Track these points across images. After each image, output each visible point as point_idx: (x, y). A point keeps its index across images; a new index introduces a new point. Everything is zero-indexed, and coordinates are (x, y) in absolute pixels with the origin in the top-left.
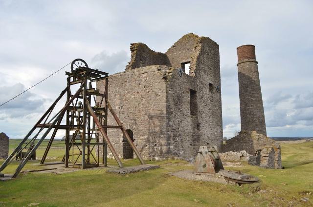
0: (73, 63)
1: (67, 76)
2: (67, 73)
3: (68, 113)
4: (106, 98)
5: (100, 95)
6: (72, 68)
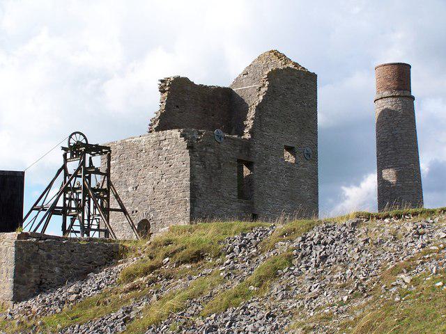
0: (70, 137)
1: (63, 152)
2: (63, 148)
3: (65, 195)
4: (109, 177)
5: (101, 174)
6: (69, 143)
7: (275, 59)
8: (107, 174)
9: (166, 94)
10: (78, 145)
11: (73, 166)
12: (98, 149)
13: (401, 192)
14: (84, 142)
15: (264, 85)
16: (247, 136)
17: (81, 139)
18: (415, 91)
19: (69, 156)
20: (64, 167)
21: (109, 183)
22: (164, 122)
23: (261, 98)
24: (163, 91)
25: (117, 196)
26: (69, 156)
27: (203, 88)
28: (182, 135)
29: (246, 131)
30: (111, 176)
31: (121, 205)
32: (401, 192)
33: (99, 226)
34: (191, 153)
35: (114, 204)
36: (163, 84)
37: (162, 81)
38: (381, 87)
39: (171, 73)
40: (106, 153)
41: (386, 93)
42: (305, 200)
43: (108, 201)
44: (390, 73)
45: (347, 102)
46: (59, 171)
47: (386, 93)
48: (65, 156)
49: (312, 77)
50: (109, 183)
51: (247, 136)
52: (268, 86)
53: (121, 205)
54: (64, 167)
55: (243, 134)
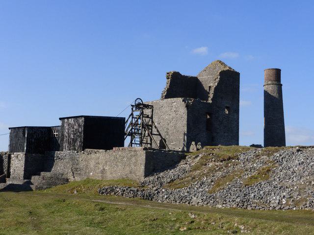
1: (132, 107)
7: (219, 64)
8: (152, 118)
9: (170, 79)
10: (139, 104)
11: (137, 113)
12: (147, 106)
13: (275, 133)
14: (141, 103)
15: (217, 78)
16: (210, 101)
17: (140, 101)
18: (282, 83)
19: (134, 109)
20: (132, 114)
21: (152, 122)
22: (170, 94)
23: (216, 84)
24: (168, 78)
25: (156, 127)
26: (134, 109)
27: (184, 76)
28: (183, 101)
29: (210, 99)
30: (154, 118)
31: (158, 131)
32: (275, 133)
33: (147, 141)
34: (187, 109)
35: (155, 131)
36: (168, 75)
37: (168, 73)
38: (268, 79)
39: (172, 71)
40: (150, 108)
41: (270, 82)
42: (233, 138)
43: (152, 129)
44: (272, 73)
45: (265, 88)
46: (130, 116)
47: (270, 82)
48: (132, 109)
49: (238, 74)
50: (152, 122)
51: (210, 101)
52: (220, 78)
53: (158, 131)
54: (132, 114)
55: (207, 100)
